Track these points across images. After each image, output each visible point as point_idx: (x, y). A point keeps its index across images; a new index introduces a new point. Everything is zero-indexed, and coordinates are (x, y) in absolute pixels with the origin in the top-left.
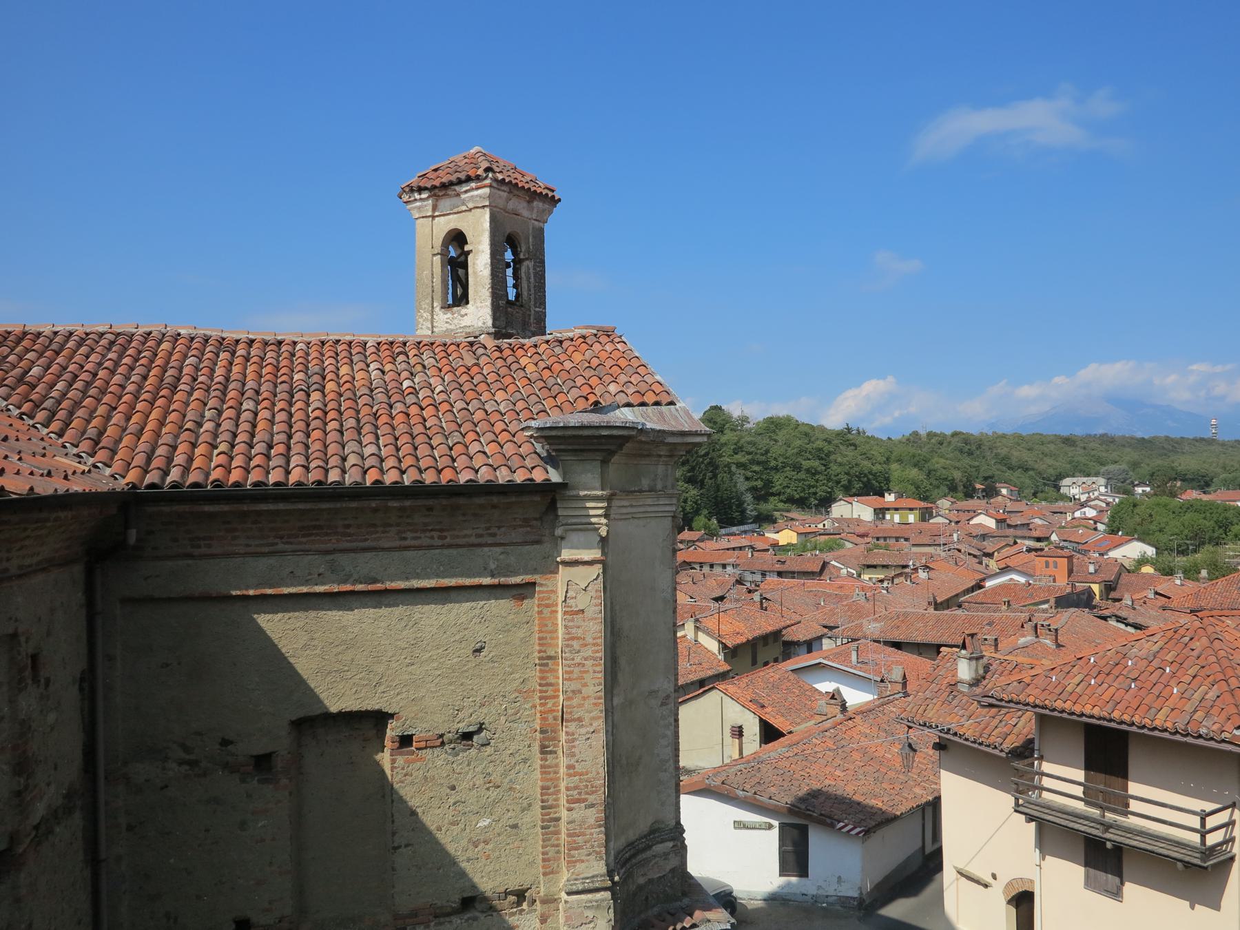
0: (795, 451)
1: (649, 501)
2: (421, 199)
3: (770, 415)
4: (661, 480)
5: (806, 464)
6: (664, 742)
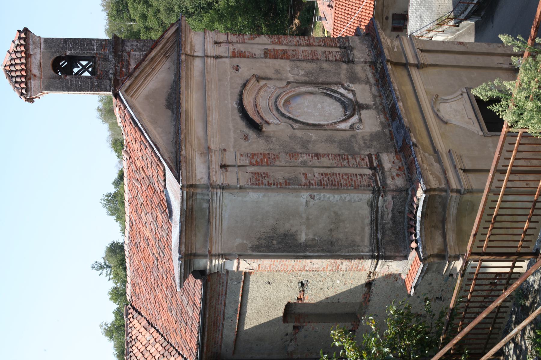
1: (214, 205)
4: (204, 196)
6: (331, 198)
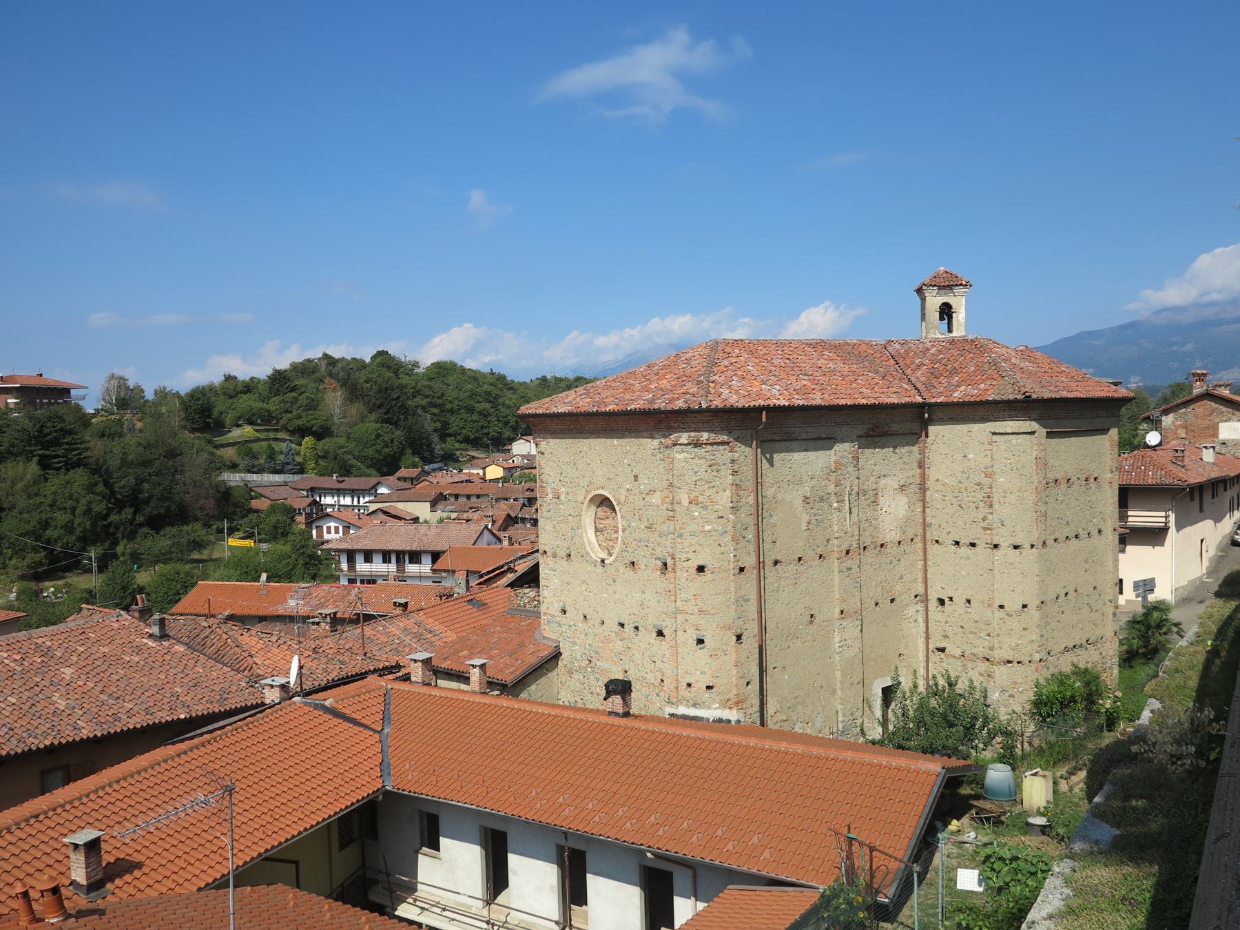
0: (467, 394)
3: (434, 361)
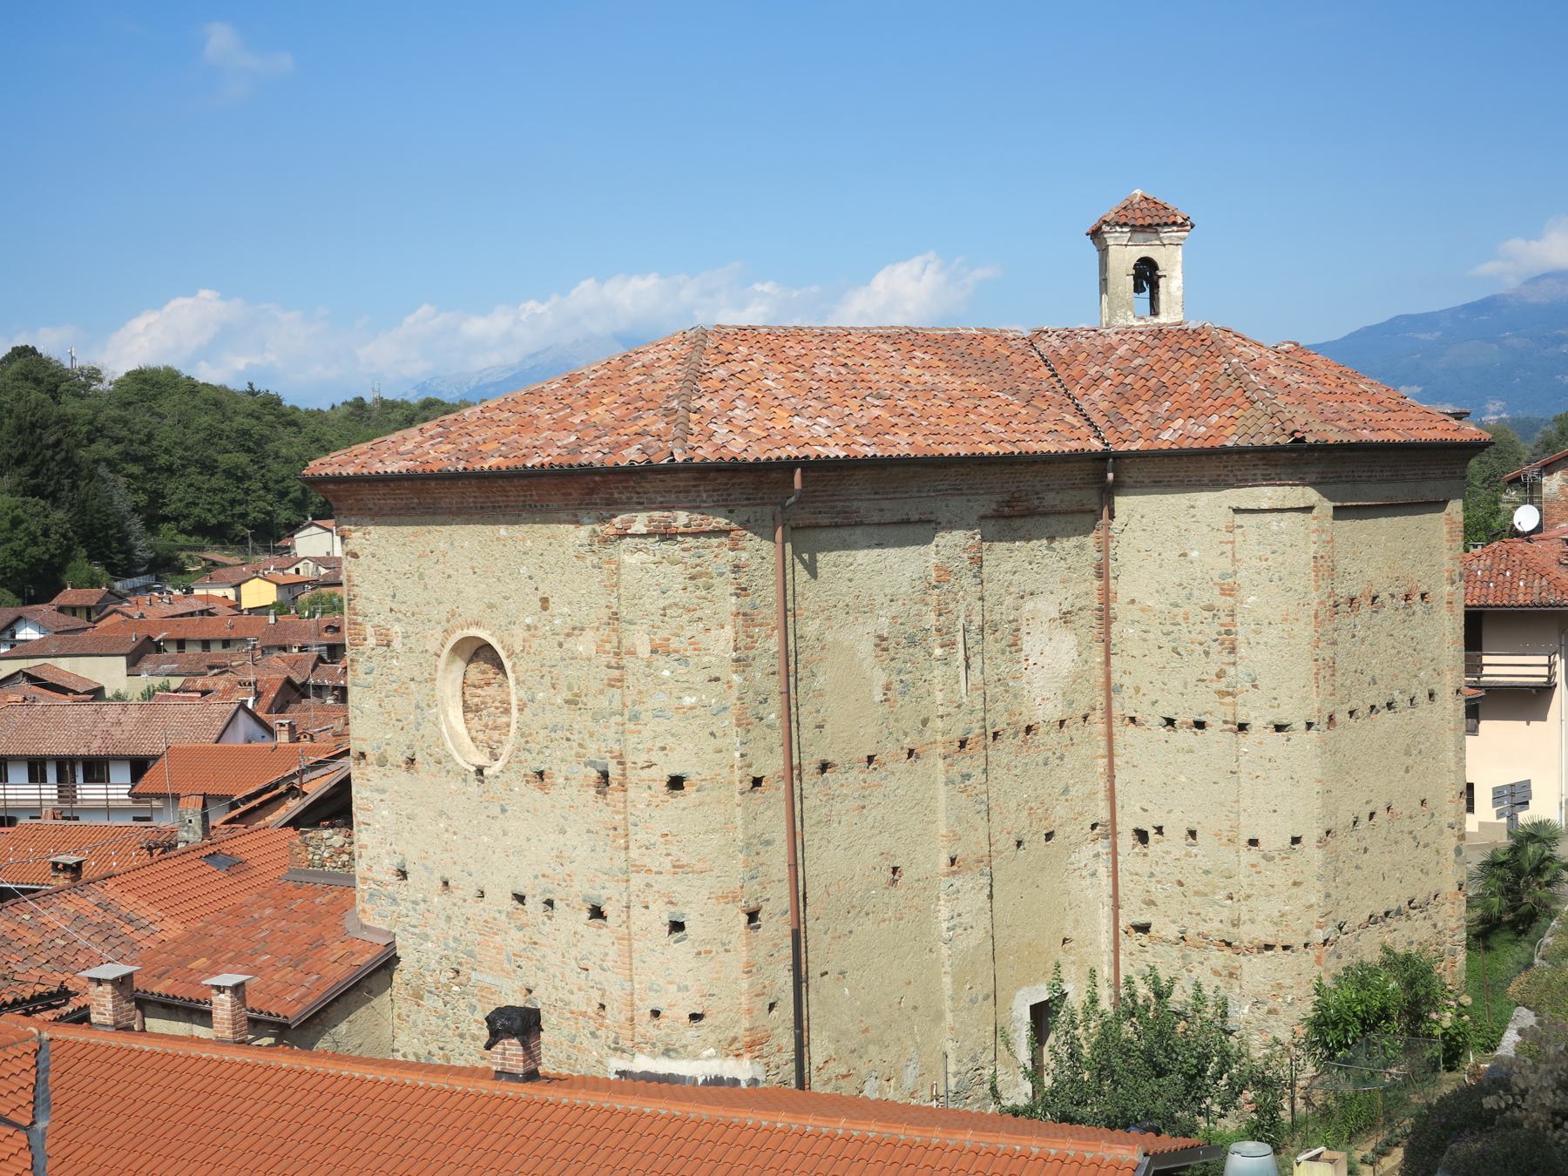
0: (202, 435)
2: (1122, 232)
5: (225, 460)
